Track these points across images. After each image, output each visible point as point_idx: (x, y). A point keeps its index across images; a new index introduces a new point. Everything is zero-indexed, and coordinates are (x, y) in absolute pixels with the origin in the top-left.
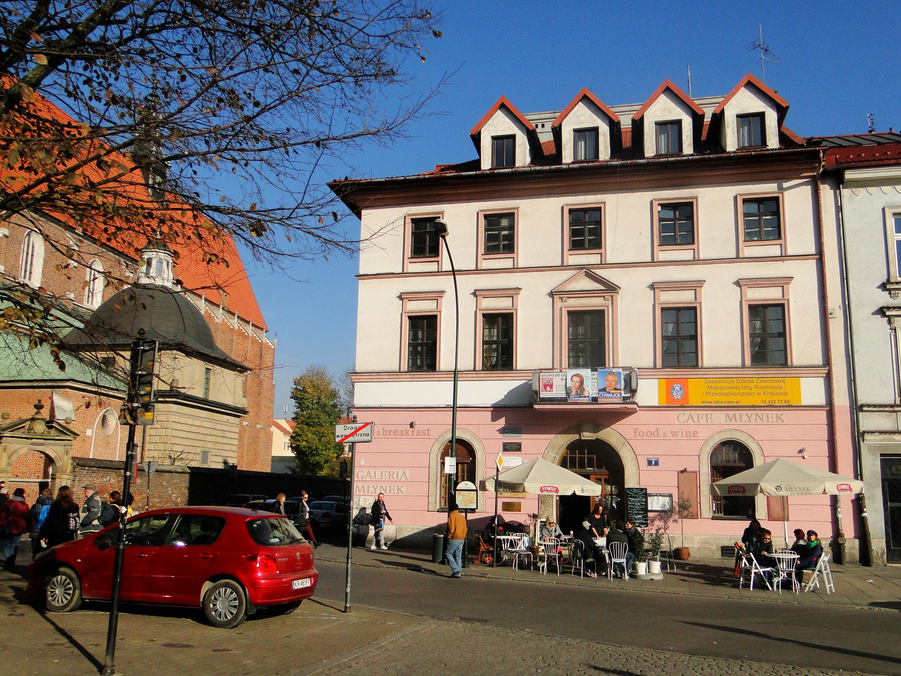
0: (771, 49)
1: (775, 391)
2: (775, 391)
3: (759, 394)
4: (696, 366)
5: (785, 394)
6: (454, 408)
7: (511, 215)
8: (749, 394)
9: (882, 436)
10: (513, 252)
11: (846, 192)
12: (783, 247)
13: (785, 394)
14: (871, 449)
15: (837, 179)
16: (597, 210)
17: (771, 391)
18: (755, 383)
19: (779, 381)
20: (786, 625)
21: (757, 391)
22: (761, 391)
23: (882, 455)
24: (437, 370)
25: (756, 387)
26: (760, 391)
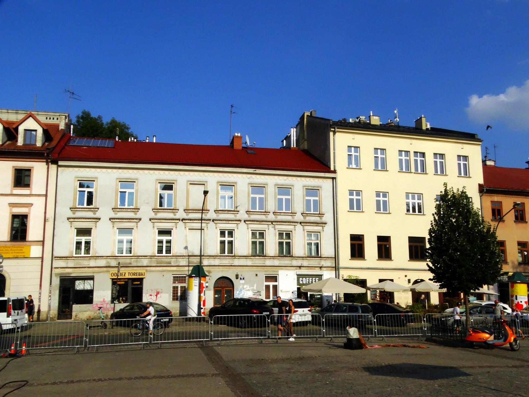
0: (75, 93)
1: (20, 251)
2: (20, 251)
3: (12, 253)
4: (26, 241)
5: (24, 253)
6: (201, 256)
7: (29, 170)
8: (8, 253)
9: (62, 269)
10: (30, 187)
11: (60, 169)
12: (31, 191)
13: (24, 253)
14: (56, 275)
15: (55, 162)
16: (29, 170)
17: (18, 251)
18: (11, 248)
19: (22, 247)
20: (494, 356)
21: (12, 251)
22: (13, 252)
23: (60, 277)
24: (27, 240)
25: (11, 250)
26: (12, 252)
